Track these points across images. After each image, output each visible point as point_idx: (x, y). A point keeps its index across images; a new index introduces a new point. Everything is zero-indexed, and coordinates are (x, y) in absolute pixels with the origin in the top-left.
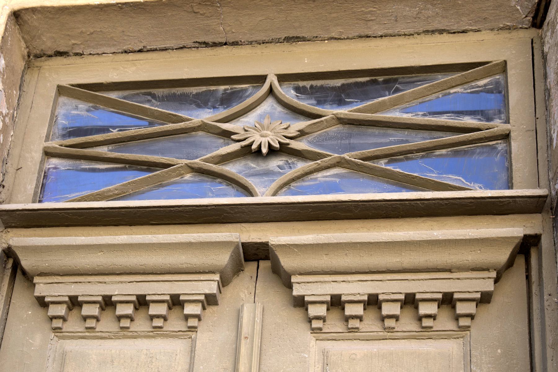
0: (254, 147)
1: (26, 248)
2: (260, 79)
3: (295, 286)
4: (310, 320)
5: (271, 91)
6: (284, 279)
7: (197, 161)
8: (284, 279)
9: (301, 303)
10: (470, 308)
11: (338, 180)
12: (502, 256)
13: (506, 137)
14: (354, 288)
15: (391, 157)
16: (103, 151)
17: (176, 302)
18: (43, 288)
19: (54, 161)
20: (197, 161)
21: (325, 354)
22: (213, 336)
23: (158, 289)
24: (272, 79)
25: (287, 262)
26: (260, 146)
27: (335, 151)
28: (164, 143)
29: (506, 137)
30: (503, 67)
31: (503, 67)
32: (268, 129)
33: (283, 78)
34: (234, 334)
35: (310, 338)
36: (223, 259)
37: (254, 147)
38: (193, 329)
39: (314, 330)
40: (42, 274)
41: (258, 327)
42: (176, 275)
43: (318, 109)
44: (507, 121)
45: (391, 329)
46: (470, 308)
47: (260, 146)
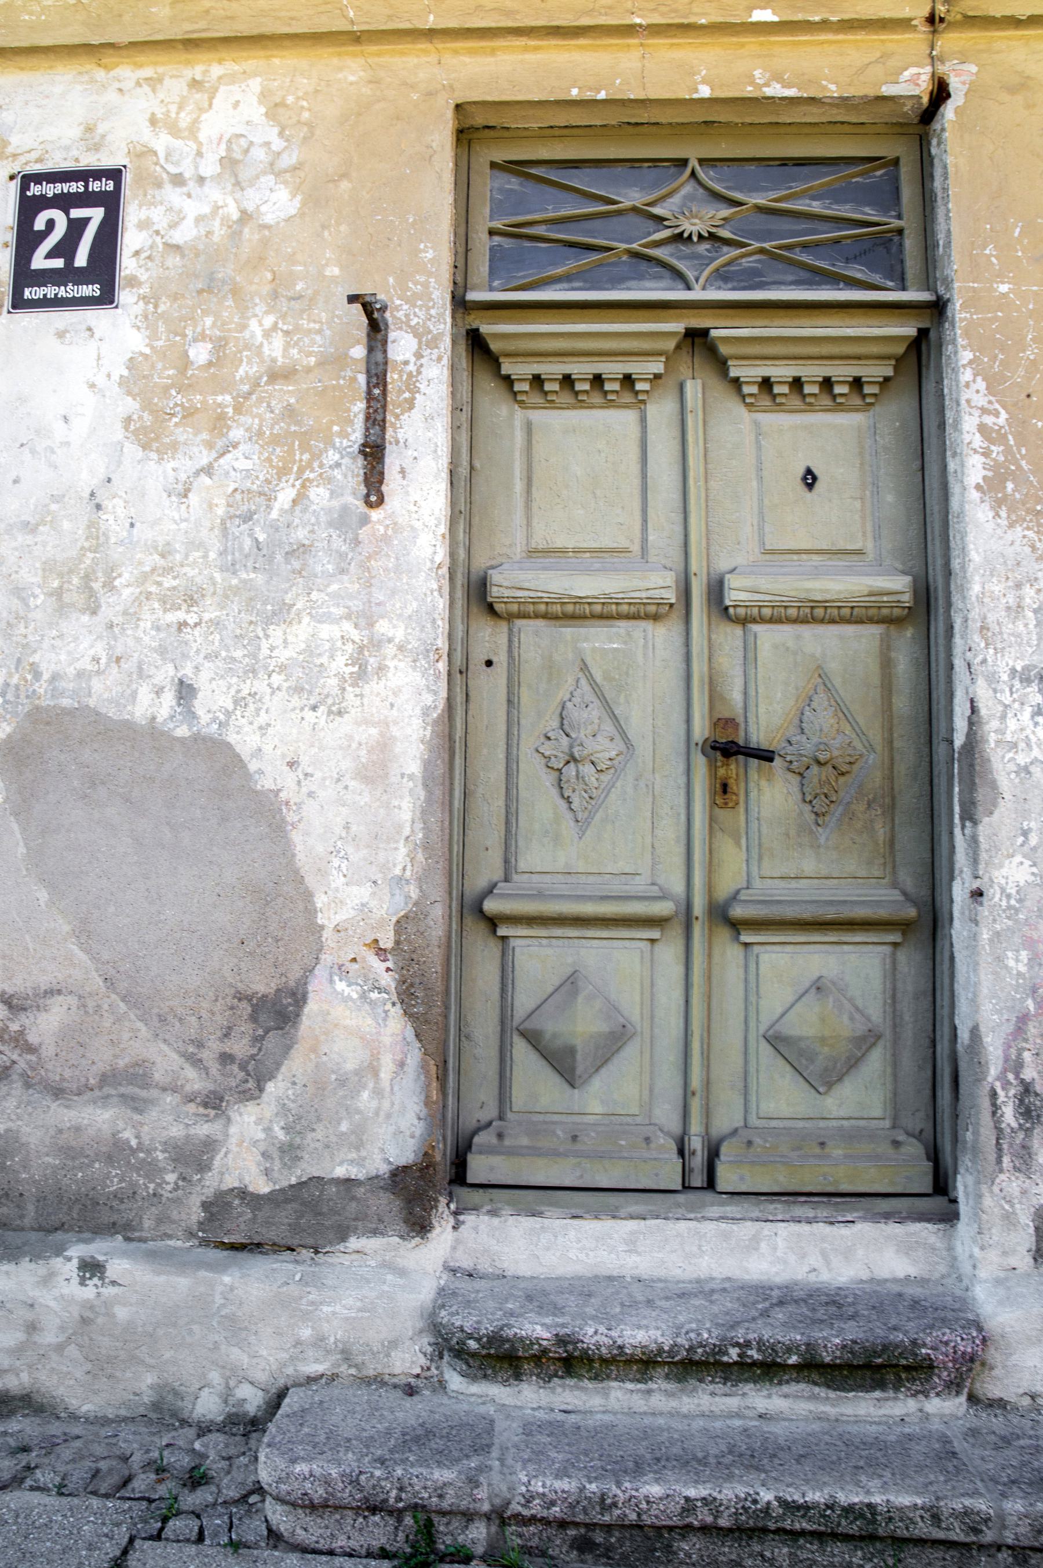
0: (686, 235)
1: (496, 336)
2: (683, 163)
3: (732, 369)
4: (744, 397)
5: (693, 174)
6: (721, 364)
7: (634, 246)
8: (721, 364)
9: (736, 382)
10: (875, 389)
11: (759, 266)
12: (900, 349)
13: (900, 232)
14: (781, 372)
15: (805, 246)
16: (540, 230)
17: (628, 380)
18: (507, 368)
19: (497, 239)
20: (635, 246)
21: (757, 424)
22: (661, 411)
23: (613, 369)
24: (693, 163)
25: (724, 350)
26: (690, 235)
27: (758, 240)
28: (597, 224)
29: (900, 232)
30: (896, 162)
31: (896, 162)
32: (696, 217)
33: (702, 161)
34: (678, 406)
35: (743, 410)
36: (671, 345)
37: (686, 235)
38: (643, 402)
39: (747, 405)
40: (508, 355)
41: (700, 403)
42: (456, 227)
43: (738, 196)
44: (899, 217)
45: (810, 404)
46: (875, 389)
47: (690, 235)
